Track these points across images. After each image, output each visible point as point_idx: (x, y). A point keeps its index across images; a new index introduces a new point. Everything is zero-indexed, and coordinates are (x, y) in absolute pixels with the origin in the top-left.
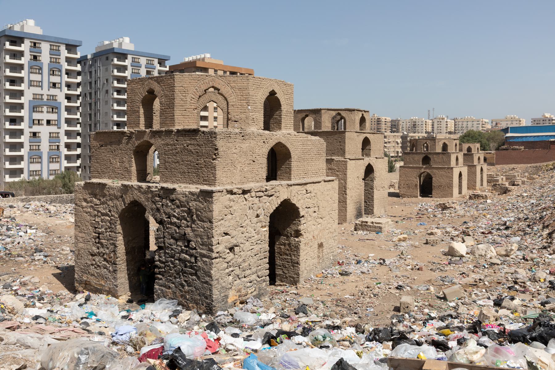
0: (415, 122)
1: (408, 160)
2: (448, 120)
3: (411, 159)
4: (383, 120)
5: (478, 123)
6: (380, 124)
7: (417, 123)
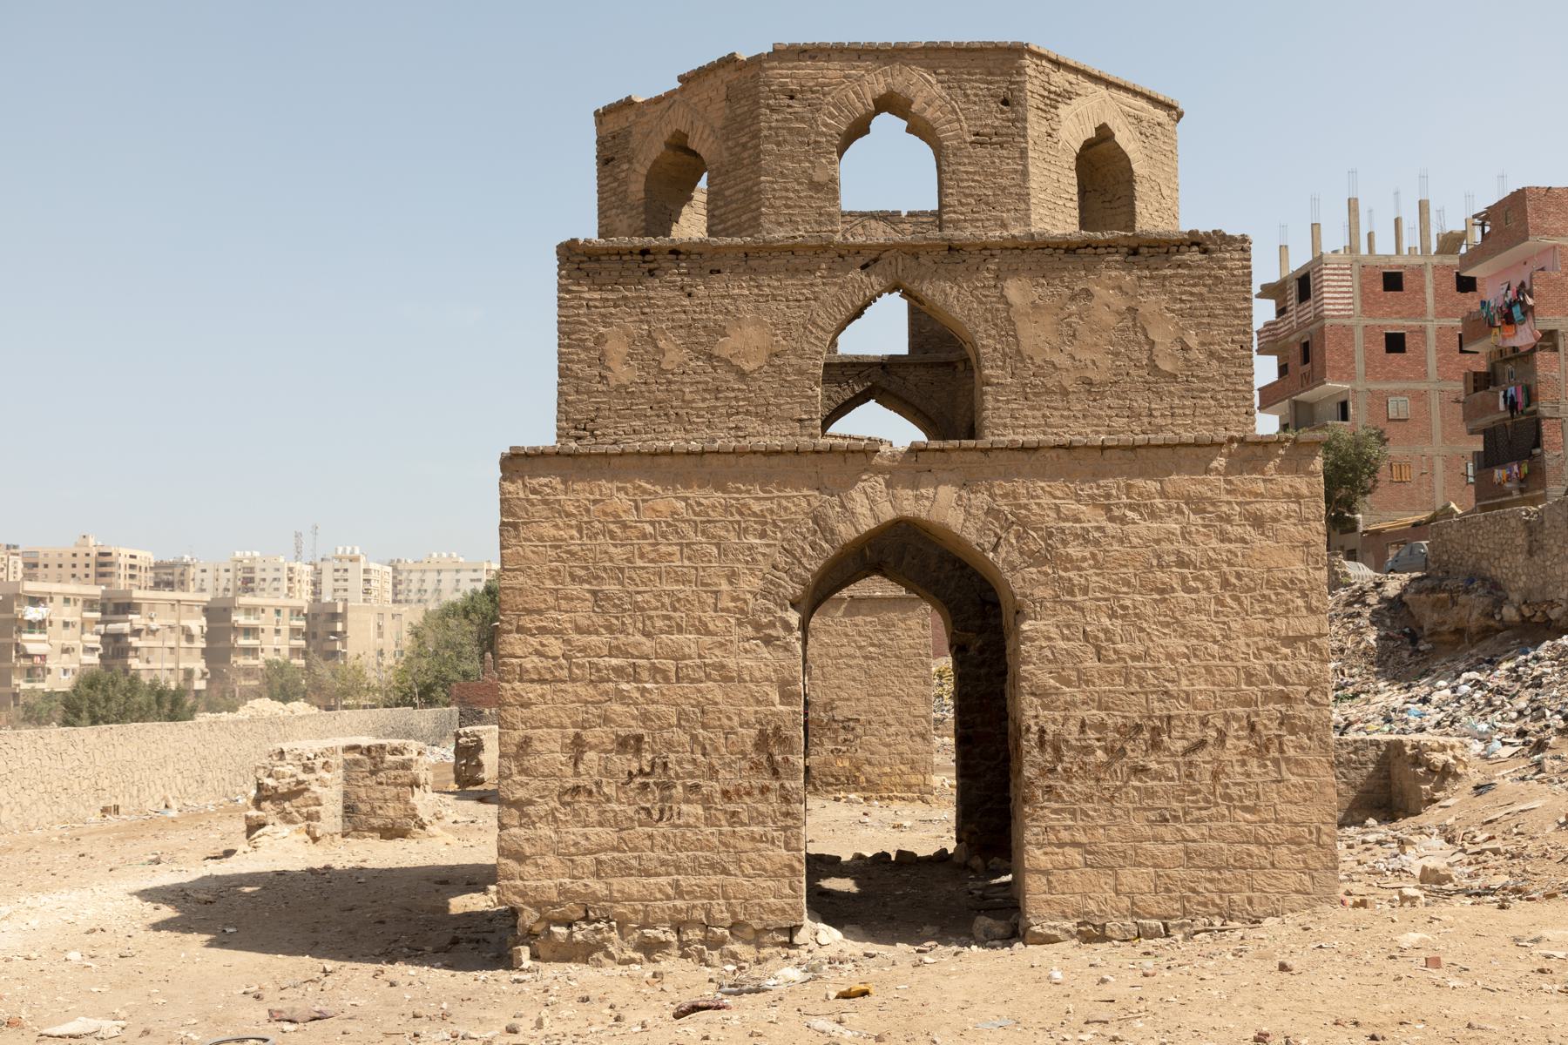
0: (251, 570)
1: (622, 373)
2: (372, 566)
3: (675, 354)
4: (122, 560)
5: (475, 575)
6: (111, 574)
7: (258, 575)
